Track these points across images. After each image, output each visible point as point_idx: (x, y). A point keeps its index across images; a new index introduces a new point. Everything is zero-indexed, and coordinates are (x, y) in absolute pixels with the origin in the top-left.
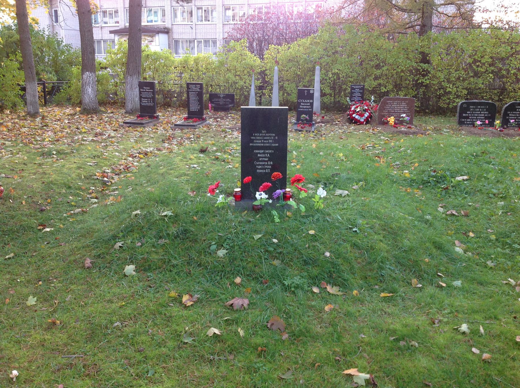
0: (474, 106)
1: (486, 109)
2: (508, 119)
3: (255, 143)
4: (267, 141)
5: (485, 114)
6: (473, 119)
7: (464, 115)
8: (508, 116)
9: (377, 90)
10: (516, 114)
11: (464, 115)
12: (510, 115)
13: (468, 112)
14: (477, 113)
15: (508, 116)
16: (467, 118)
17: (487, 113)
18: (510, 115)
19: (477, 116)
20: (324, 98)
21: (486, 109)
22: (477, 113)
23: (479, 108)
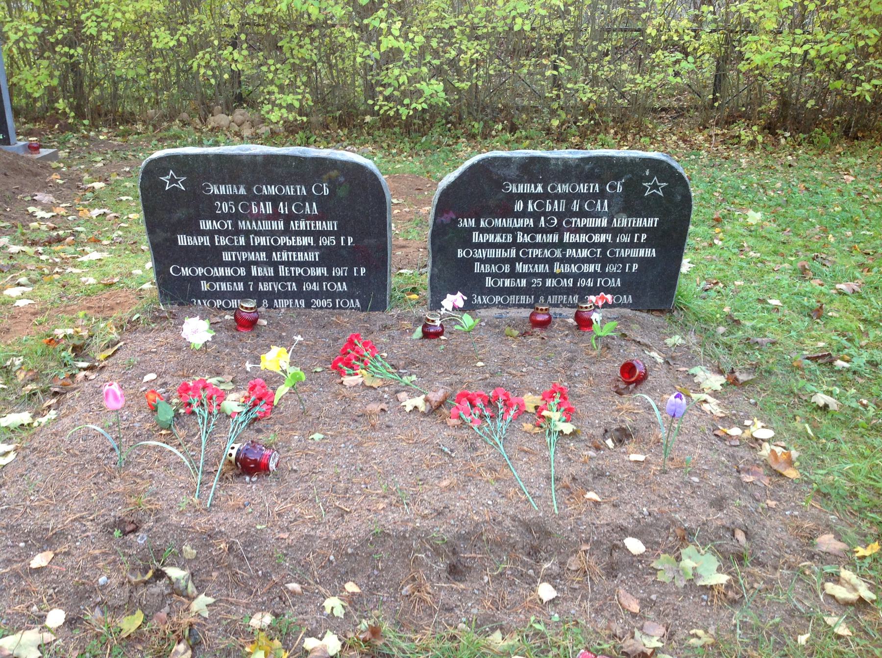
0: (234, 180)
1: (322, 201)
2: (469, 263)
3: (480, 246)
4: (584, 238)
5: (316, 235)
6: (247, 264)
7: (183, 240)
8: (467, 243)
9: (386, 111)
10: (513, 231)
11: (183, 240)
12: (476, 237)
13: (206, 225)
14: (266, 225)
15: (467, 243)
16: (210, 256)
17: (330, 226)
18: (476, 237)
19: (269, 250)
20: (205, 142)
21: (322, 201)
22: (266, 225)
23: (275, 200)
